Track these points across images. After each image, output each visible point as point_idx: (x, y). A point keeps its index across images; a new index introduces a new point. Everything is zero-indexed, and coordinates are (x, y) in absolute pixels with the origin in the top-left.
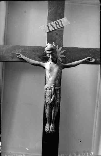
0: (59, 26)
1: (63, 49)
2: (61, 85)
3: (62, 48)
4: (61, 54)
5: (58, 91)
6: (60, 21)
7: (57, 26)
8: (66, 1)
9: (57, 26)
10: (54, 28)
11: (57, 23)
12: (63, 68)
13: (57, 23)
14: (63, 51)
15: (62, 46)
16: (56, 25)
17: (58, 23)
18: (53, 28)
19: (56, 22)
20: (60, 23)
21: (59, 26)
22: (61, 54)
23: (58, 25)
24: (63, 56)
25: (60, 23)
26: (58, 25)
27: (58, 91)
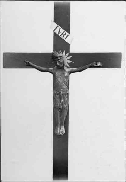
0: (63, 37)
1: (70, 54)
2: (69, 89)
3: (69, 54)
4: (68, 60)
5: (66, 95)
6: (67, 35)
7: (62, 35)
8: (2, 1)
9: (62, 35)
10: (59, 33)
11: (64, 34)
12: (70, 74)
13: (64, 34)
14: (70, 57)
15: (69, 51)
16: (62, 34)
17: (65, 34)
18: (58, 32)
19: (64, 32)
20: (65, 36)
21: (63, 37)
22: (68, 60)
23: (63, 35)
24: (70, 57)
25: (65, 36)
26: (63, 35)
27: (66, 95)
